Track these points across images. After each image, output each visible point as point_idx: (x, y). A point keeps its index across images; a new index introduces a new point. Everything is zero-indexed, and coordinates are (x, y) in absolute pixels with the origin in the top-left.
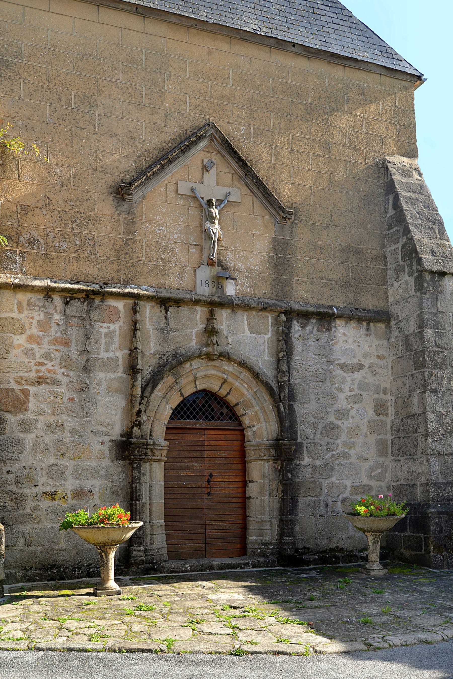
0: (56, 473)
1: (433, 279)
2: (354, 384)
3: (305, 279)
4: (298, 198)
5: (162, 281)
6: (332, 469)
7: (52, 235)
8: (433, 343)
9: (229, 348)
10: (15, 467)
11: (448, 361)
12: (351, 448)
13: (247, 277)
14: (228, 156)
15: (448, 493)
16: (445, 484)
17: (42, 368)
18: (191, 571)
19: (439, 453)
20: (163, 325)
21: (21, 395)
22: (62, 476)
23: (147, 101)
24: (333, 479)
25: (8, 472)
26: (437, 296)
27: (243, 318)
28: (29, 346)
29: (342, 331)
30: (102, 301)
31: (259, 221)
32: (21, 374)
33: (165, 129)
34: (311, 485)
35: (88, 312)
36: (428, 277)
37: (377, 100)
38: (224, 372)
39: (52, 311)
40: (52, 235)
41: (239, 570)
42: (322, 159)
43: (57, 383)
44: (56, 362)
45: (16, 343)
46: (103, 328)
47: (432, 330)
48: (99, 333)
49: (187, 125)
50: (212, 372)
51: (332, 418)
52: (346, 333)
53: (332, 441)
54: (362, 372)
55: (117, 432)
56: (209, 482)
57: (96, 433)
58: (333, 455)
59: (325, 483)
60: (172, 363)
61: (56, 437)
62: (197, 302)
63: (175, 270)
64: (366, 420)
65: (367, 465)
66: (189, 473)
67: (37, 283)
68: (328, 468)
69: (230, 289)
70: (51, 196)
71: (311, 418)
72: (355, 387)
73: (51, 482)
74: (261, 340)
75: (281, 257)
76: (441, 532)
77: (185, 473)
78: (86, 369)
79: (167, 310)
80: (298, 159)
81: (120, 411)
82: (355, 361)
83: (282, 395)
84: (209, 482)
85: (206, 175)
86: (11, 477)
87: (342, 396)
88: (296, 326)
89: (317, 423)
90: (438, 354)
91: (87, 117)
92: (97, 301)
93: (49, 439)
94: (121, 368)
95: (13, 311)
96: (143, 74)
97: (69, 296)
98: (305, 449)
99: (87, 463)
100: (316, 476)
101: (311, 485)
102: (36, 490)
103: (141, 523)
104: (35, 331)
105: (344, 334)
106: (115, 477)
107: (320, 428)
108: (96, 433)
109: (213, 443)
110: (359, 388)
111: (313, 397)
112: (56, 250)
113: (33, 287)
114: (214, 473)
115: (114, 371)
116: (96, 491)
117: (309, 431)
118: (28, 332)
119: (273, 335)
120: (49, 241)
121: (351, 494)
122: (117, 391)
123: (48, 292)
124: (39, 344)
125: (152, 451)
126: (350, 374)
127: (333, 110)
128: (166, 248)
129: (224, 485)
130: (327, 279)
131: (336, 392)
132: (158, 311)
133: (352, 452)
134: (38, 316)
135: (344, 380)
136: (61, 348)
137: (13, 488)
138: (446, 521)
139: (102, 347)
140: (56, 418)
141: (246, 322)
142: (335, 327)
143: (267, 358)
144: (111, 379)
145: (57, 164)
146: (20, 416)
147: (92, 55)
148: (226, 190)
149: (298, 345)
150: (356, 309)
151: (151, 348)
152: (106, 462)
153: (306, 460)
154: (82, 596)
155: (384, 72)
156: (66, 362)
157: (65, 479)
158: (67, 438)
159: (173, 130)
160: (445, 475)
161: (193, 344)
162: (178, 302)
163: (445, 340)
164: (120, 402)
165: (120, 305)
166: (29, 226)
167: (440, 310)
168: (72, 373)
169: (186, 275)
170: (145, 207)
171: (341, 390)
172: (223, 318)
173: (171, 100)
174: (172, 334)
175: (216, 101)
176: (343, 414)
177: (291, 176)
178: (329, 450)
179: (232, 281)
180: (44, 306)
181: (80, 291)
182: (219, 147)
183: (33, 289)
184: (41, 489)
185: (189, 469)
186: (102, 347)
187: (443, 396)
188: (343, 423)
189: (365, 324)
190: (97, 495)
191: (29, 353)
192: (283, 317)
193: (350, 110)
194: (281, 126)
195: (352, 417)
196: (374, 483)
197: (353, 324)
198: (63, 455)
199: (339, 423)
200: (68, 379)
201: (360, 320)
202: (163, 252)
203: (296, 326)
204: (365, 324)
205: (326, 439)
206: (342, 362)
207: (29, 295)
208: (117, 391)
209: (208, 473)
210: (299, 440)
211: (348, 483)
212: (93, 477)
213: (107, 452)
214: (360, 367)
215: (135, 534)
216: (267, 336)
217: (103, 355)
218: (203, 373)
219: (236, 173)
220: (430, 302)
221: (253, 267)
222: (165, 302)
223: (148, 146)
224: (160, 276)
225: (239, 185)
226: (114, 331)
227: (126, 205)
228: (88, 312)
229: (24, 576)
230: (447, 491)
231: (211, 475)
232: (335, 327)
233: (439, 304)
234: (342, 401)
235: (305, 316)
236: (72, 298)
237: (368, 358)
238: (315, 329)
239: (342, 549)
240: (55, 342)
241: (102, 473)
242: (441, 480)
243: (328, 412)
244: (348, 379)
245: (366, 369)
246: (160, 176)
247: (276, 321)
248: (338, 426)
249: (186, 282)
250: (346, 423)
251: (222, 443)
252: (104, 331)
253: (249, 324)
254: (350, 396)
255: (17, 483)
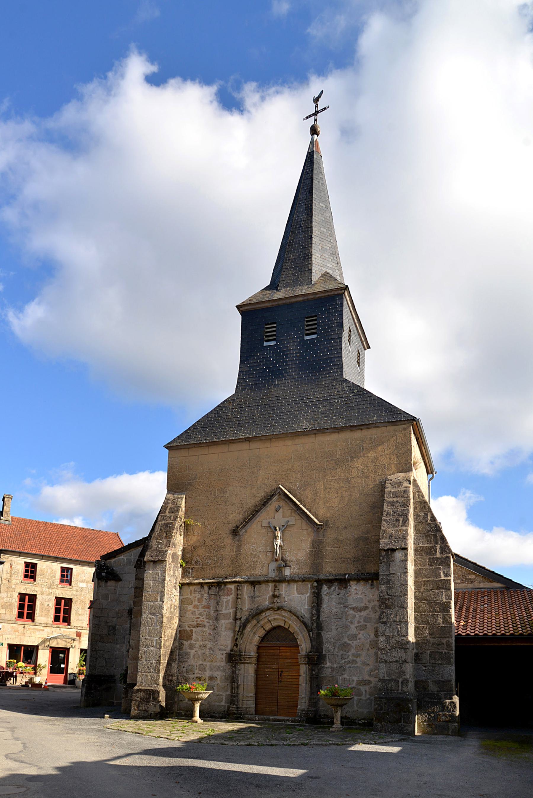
0: (202, 668)
1: (387, 555)
2: (361, 619)
3: (331, 560)
4: (328, 514)
5: (253, 572)
6: (344, 670)
7: (205, 558)
8: (386, 594)
9: (285, 604)
10: (186, 665)
11: (396, 604)
12: (357, 657)
13: (297, 564)
14: (288, 501)
15: (391, 686)
16: (389, 681)
17: (199, 620)
18: (258, 720)
19: (386, 661)
20: (252, 595)
21: (190, 632)
22: (204, 670)
23: (249, 483)
24: (345, 676)
25: (183, 667)
26: (389, 564)
27: (294, 587)
28: (194, 610)
29: (354, 588)
30: (225, 586)
31: (305, 532)
32: (190, 623)
33: (257, 495)
34: (331, 679)
35: (218, 592)
36: (384, 553)
37: (383, 443)
38: (284, 616)
39: (203, 593)
40: (205, 558)
41: (284, 723)
42: (344, 489)
43: (204, 626)
44: (204, 617)
45: (189, 609)
46: (224, 599)
47: (385, 585)
48: (223, 601)
49: (268, 490)
50: (277, 617)
51: (346, 640)
52: (358, 588)
53: (345, 653)
54: (367, 611)
55: (228, 649)
56: (281, 675)
57: (220, 650)
58: (345, 662)
59: (340, 678)
60: (256, 614)
61: (203, 651)
62: (267, 581)
63: (259, 566)
64: (368, 641)
65: (368, 668)
66: (270, 670)
67: (196, 581)
68: (342, 669)
69: (287, 572)
70: (206, 539)
71: (332, 640)
72: (362, 620)
73: (200, 672)
74: (303, 598)
75: (317, 552)
76: (381, 709)
77: (268, 670)
78: (217, 619)
79: (254, 587)
80: (329, 492)
81: (230, 639)
82: (363, 605)
83: (315, 627)
84: (281, 675)
85: (277, 514)
86: (184, 669)
87: (353, 626)
88: (325, 588)
89: (335, 643)
90: (389, 600)
91: (222, 499)
92: (223, 586)
93: (200, 652)
94: (232, 618)
95: (188, 595)
96: (248, 470)
97: (210, 585)
98: (327, 657)
99: (215, 664)
100: (334, 673)
101: (331, 679)
102: (193, 676)
103: (211, 692)
104: (196, 603)
105: (356, 589)
106: (227, 671)
107: (337, 646)
108: (220, 650)
109: (283, 654)
110: (364, 621)
111: (333, 628)
112: (206, 564)
113: (194, 583)
114: (284, 670)
115: (229, 619)
116: (218, 677)
117: (331, 648)
118: (194, 604)
119: (310, 594)
120: (204, 561)
121: (357, 685)
122: (229, 629)
123: (201, 584)
124: (198, 608)
125: (244, 658)
126: (359, 613)
127: (352, 458)
128: (255, 555)
129: (289, 677)
130: (345, 558)
131: (349, 624)
132: (250, 587)
133: (358, 660)
134: (198, 596)
135: (354, 617)
136: (206, 610)
137: (185, 674)
138: (385, 703)
139: (224, 608)
140: (203, 643)
141: (295, 589)
142: (350, 586)
143: (306, 607)
144: (227, 623)
145: (209, 524)
146: (189, 642)
147: (225, 468)
148: (287, 519)
149: (325, 599)
150: (362, 574)
151: (246, 606)
152: (224, 664)
153: (328, 664)
154: (183, 723)
155: (388, 424)
156: (208, 617)
157: (206, 671)
158: (207, 652)
159: (261, 494)
160: (389, 674)
161: (267, 603)
162: (259, 583)
163: (394, 590)
164: (230, 634)
165: (232, 587)
166: (196, 555)
167: (391, 572)
168: (210, 621)
169: (265, 569)
170: (246, 537)
171: (352, 623)
172: (283, 588)
173: (261, 480)
174: (257, 599)
175: (284, 473)
176: (354, 637)
177: (324, 503)
178: (342, 659)
179: (288, 568)
180: (200, 591)
181: (213, 583)
182: (283, 498)
183: (194, 584)
184: (196, 675)
185: (271, 668)
186: (224, 608)
187: (390, 625)
188: (353, 643)
189: (370, 582)
190: (219, 679)
191: (194, 613)
192: (315, 584)
193: (364, 454)
194: (320, 476)
195: (359, 639)
196: (371, 679)
197: (362, 583)
198: (205, 660)
199: (350, 642)
200: (209, 624)
201: (366, 580)
202: (254, 558)
203: (325, 588)
204: (370, 582)
205: (342, 652)
206: (354, 606)
207: (195, 587)
208: (229, 629)
209: (280, 670)
210: (324, 653)
211: (355, 678)
212: (218, 670)
213: (224, 659)
214: (366, 608)
215: (209, 695)
216: (307, 595)
217: (224, 612)
218: (272, 618)
219: (293, 509)
220: (384, 569)
221: (300, 558)
222: (253, 583)
223: (249, 505)
224: (252, 570)
225: (295, 515)
226: (229, 600)
227: (237, 538)
228: (218, 592)
229: (185, 714)
230: (390, 685)
231: (282, 672)
232: (350, 586)
233: (391, 569)
234: (353, 630)
235: (330, 582)
236: (212, 586)
237: (372, 602)
238: (337, 588)
239: (349, 718)
240: (204, 607)
241: (222, 669)
242: (386, 678)
243: (343, 636)
244: (357, 616)
245: (370, 609)
246: (253, 520)
247: (312, 587)
248: (349, 644)
249: (264, 571)
250: (355, 642)
251: (288, 654)
252: (225, 600)
253: (297, 589)
254: (358, 626)
255: (187, 672)
